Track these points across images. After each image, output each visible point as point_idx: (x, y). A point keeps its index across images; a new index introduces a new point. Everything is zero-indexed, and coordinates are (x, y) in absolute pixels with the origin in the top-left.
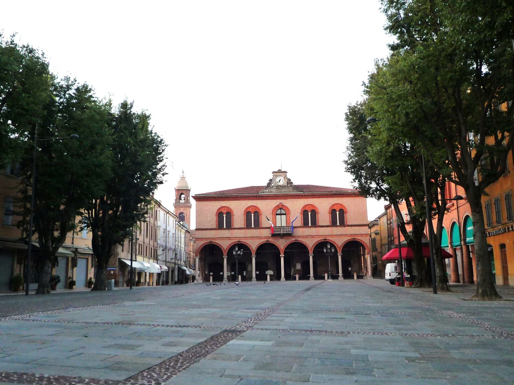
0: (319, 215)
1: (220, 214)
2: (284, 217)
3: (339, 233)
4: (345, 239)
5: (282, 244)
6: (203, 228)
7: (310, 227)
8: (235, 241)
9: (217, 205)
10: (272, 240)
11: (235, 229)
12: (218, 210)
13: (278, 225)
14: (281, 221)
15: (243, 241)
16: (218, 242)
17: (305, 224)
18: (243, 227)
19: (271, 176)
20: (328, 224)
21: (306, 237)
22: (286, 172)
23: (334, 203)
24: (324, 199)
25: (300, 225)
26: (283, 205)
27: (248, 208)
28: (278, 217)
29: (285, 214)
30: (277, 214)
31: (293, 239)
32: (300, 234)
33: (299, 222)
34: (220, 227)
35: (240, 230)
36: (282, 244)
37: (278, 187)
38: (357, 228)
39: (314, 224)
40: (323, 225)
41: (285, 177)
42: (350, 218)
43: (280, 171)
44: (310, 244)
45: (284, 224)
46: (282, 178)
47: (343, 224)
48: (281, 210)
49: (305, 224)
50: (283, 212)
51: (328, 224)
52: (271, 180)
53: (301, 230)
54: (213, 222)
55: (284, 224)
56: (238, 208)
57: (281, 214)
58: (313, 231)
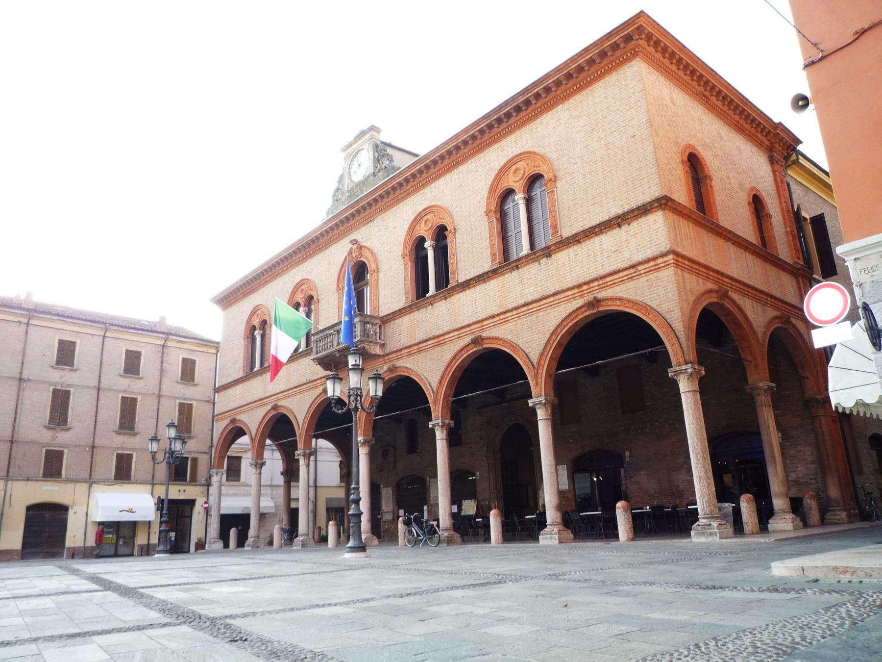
8: (461, 343)
11: (467, 285)
21: (502, 316)
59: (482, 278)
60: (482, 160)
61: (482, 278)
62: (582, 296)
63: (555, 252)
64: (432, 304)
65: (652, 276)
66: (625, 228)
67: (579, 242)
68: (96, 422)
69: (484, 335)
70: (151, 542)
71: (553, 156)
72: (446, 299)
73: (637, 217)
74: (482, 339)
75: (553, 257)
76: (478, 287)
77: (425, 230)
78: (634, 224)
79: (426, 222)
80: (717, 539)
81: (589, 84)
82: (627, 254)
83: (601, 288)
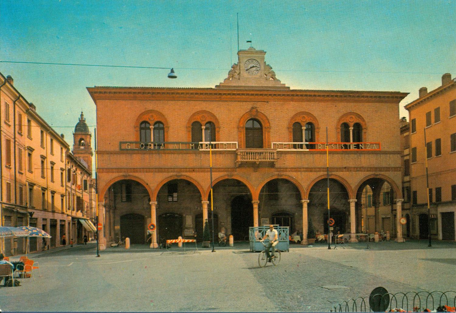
1: (143, 126)
4: (314, 176)
9: (344, 107)
10: (238, 175)
44: (305, 182)
58: (156, 160)
71: (220, 122)
77: (352, 121)
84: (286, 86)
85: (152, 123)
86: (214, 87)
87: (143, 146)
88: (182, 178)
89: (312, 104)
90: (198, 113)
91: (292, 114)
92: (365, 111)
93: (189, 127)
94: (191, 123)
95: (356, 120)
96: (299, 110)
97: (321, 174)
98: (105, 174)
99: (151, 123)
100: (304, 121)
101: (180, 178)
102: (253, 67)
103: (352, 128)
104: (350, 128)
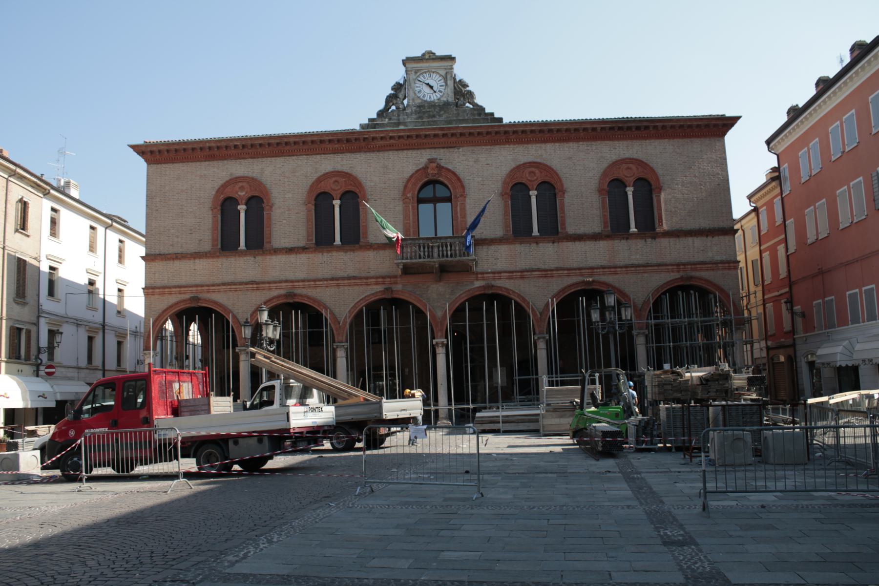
0: (568, 199)
1: (226, 206)
2: (444, 208)
3: (637, 258)
4: (659, 280)
5: (439, 300)
6: (171, 250)
7: (537, 240)
8: (275, 293)
9: (219, 173)
10: (402, 289)
11: (276, 251)
12: (219, 191)
13: (426, 232)
14: (438, 221)
15: (304, 292)
16: (504, 284)
17: (519, 230)
18: (301, 244)
19: (399, 74)
20: (595, 226)
21: (523, 274)
22: (451, 59)
23: (614, 158)
24: (583, 146)
25: (499, 232)
26: (440, 168)
27: (319, 180)
28: (426, 209)
29: (448, 199)
30: (420, 201)
31: (478, 284)
32: (501, 266)
33: (494, 224)
34: (227, 244)
35: (292, 258)
36: (439, 300)
37: (424, 109)
38: (698, 242)
39: (552, 229)
40: (581, 230)
41: (448, 75)
42: (670, 208)
43: (429, 57)
44: (540, 297)
45: (445, 230)
46: (435, 81)
47: (649, 226)
48: (433, 188)
49: (519, 230)
50: (441, 192)
51: (595, 226)
52: (398, 87)
53: (503, 250)
54: (202, 226)
55: (445, 230)
56: (288, 188)
57: (435, 200)
58: (547, 254)
59: (291, 251)
60: (594, 148)
61: (291, 251)
62: (678, 272)
63: (659, 237)
64: (537, 243)
65: (726, 272)
66: (710, 238)
67: (678, 236)
68: (6, 212)
69: (200, 296)
70: (480, 451)
71: (660, 172)
72: (553, 242)
73: (719, 235)
74: (295, 295)
75: (658, 240)
76: (588, 242)
77: (336, 188)
78: (716, 238)
79: (336, 181)
80: (640, 417)
81: (690, 137)
82: (710, 254)
83: (692, 270)
84: (496, 116)
85: (337, 193)
86: (358, 128)
87: (227, 244)
88: (297, 300)
89: (549, 146)
90: (525, 165)
91: (505, 170)
92: (655, 153)
93: (506, 194)
94: (608, 180)
95: (539, 177)
96: (523, 159)
97: (374, 290)
98: (157, 297)
99: (333, 194)
100: (629, 175)
101: (590, 287)
102: (431, 87)
103: (536, 192)
104: (628, 189)
